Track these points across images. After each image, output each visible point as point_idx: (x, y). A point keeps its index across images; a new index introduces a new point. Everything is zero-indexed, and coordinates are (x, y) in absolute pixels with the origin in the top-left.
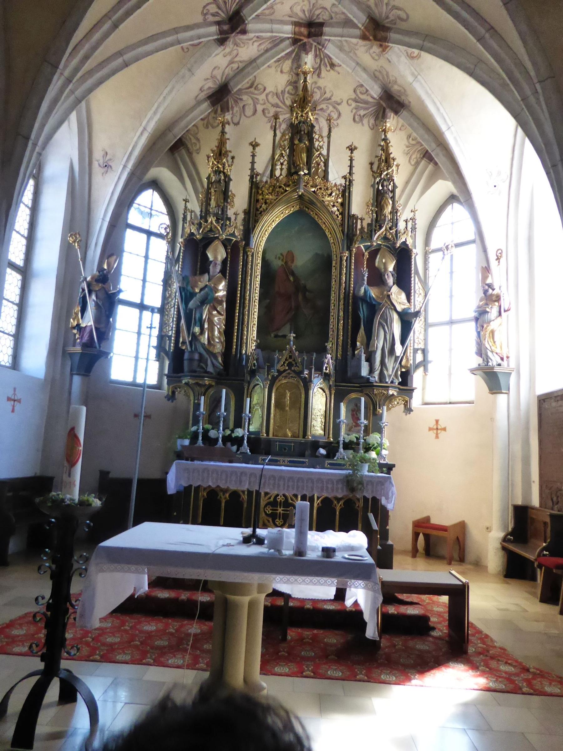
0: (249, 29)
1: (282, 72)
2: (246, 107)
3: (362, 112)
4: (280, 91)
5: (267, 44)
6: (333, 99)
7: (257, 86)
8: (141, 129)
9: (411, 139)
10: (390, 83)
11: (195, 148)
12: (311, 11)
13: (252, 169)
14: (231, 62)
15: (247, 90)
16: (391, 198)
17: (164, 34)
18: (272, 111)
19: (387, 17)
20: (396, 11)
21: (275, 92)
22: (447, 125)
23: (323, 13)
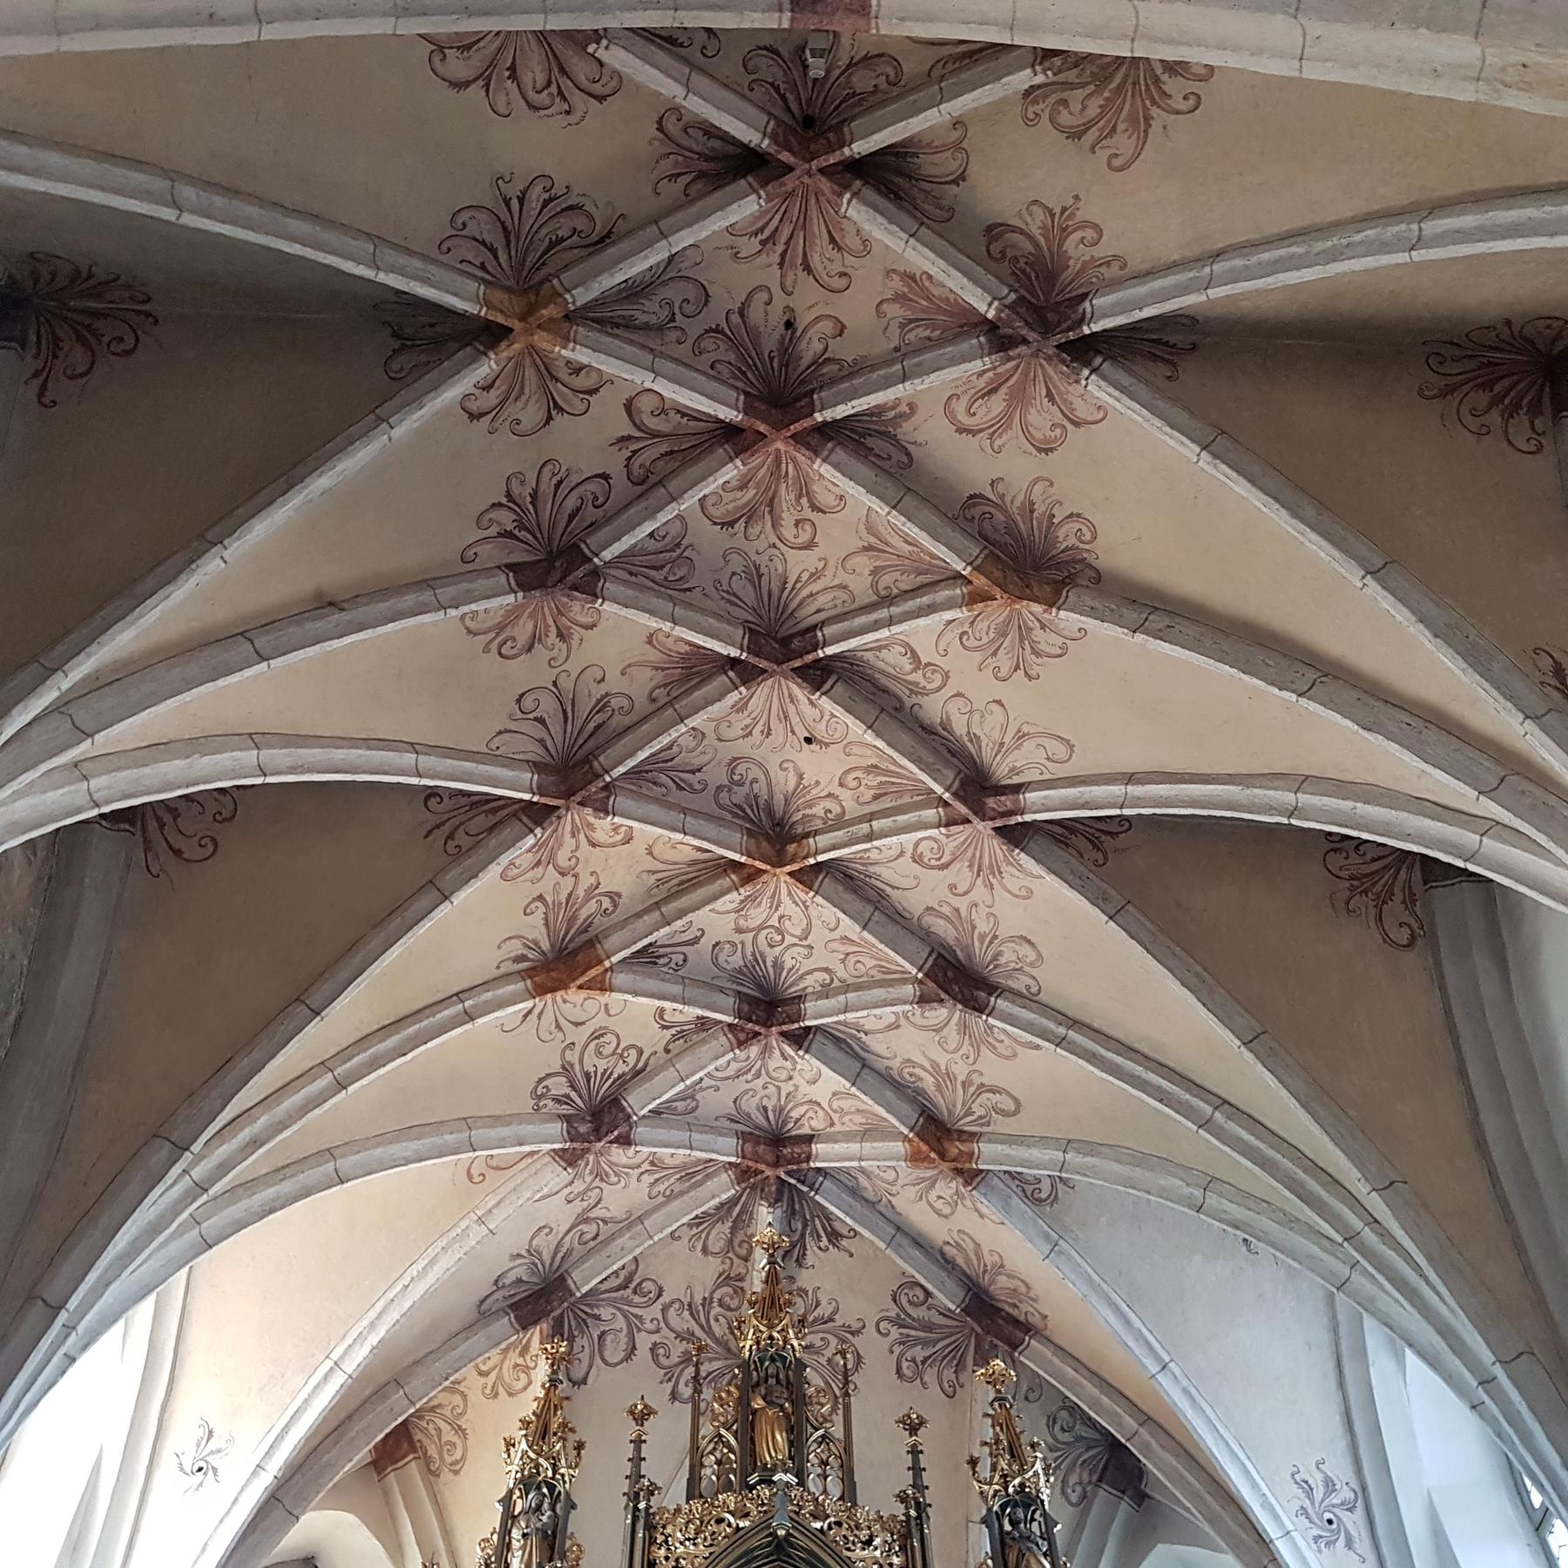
0: (637, 1138)
1: (705, 1250)
2: (609, 1338)
3: (919, 1353)
4: (698, 1300)
5: (672, 1180)
6: (839, 1320)
7: (640, 1284)
8: (329, 1364)
9: (1057, 1427)
10: (985, 1272)
11: (449, 1460)
12: (782, 1109)
13: (636, 1476)
14: (584, 1219)
15: (614, 1295)
16: (1045, 1555)
17: (439, 1126)
18: (678, 1348)
19: (969, 1113)
20: (990, 1095)
21: (686, 1300)
22: (1158, 1358)
23: (810, 1114)
